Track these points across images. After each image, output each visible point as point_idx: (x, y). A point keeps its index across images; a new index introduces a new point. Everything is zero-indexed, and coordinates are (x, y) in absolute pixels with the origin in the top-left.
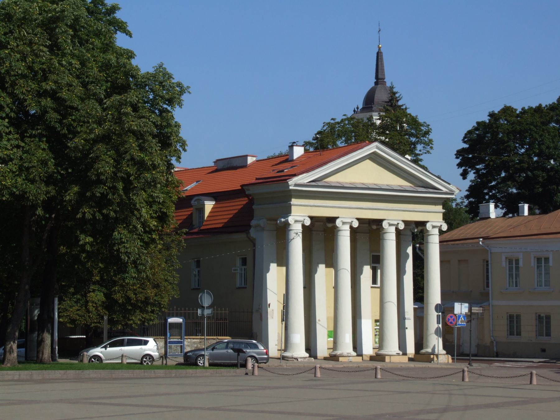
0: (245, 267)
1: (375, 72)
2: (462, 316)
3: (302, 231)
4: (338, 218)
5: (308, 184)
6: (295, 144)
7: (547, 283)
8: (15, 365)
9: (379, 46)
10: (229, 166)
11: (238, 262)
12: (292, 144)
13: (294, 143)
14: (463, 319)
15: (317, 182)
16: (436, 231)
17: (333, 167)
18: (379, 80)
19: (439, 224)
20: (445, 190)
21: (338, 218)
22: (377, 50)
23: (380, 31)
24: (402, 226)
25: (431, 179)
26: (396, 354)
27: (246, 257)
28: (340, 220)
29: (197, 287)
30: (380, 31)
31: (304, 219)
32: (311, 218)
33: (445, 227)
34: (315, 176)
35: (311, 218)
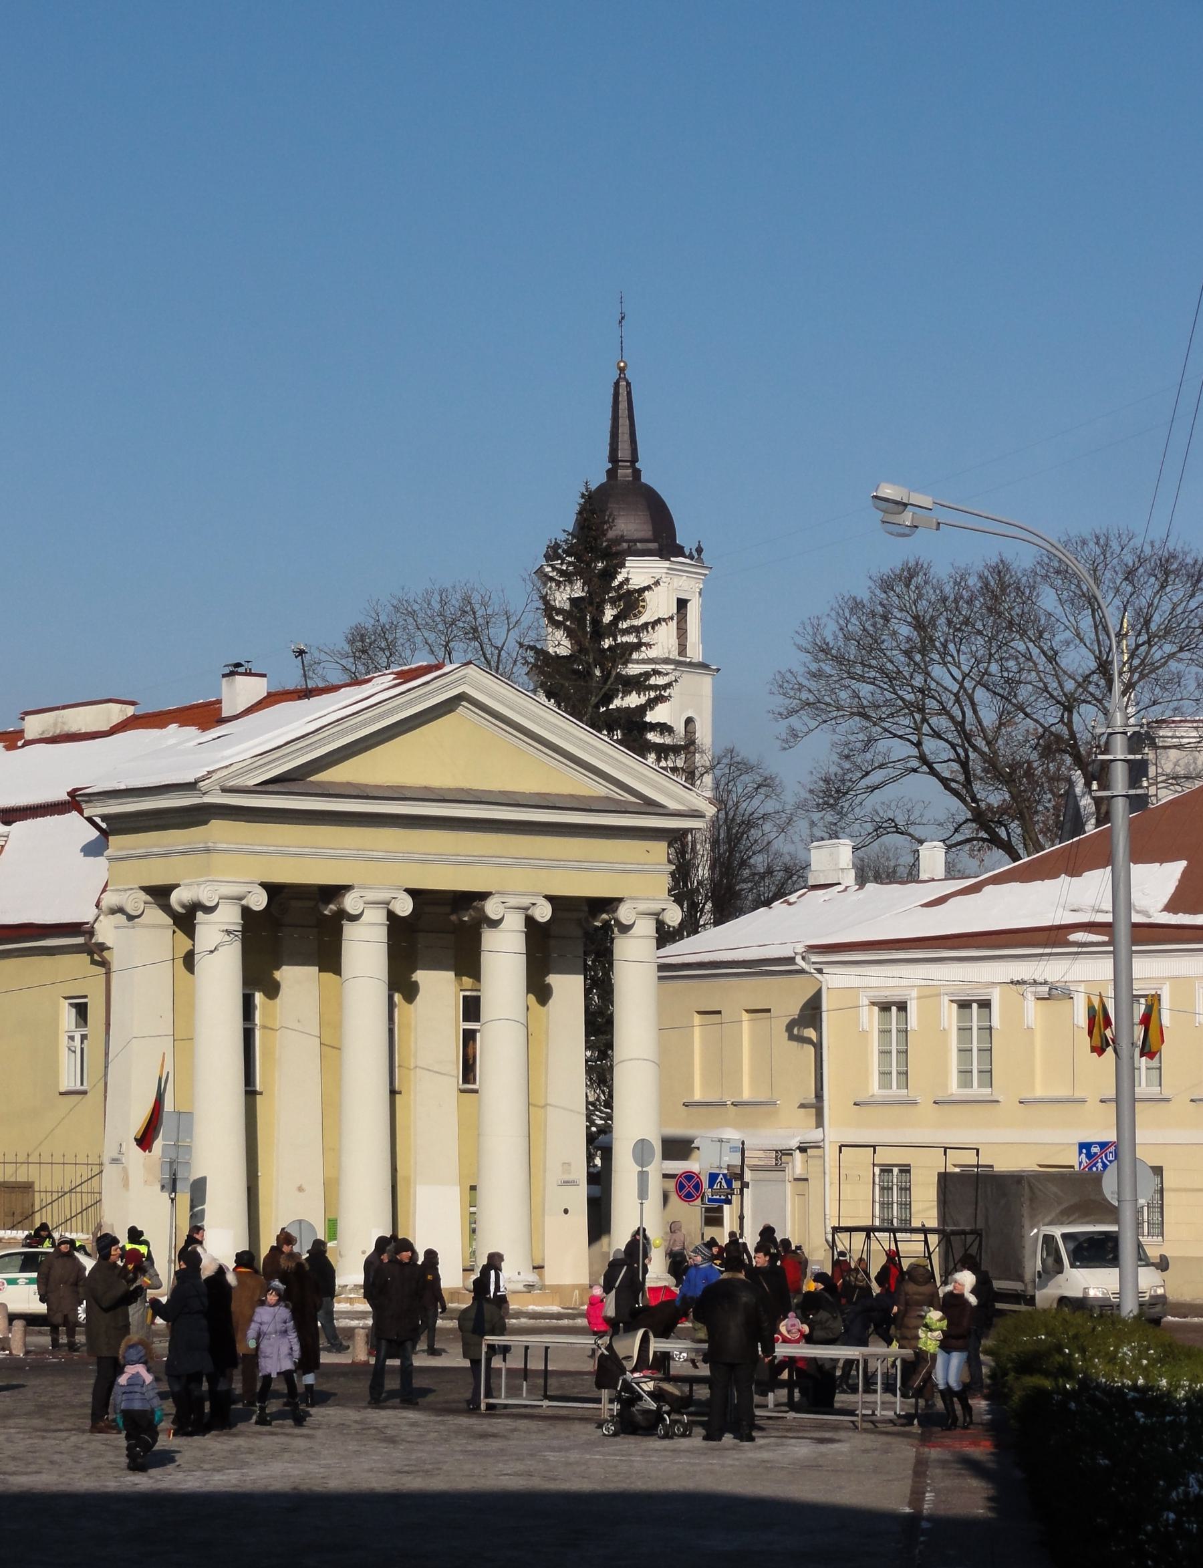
0: (84, 1031)
1: (608, 440)
2: (721, 1176)
3: (243, 926)
4: (348, 888)
5: (259, 788)
6: (241, 670)
7: (987, 1075)
8: (1122, 1373)
9: (618, 364)
10: (58, 732)
11: (68, 1016)
12: (231, 668)
13: (238, 665)
14: (724, 1183)
15: (286, 784)
16: (646, 928)
17: (333, 741)
18: (620, 464)
19: (656, 907)
20: (672, 805)
22: (615, 375)
23: (623, 318)
24: (544, 913)
25: (638, 778)
26: (524, 1289)
27: (479, 994)
28: (358, 895)
29: (78, 1087)
30: (623, 318)
32: (272, 889)
33: (674, 916)
34: (282, 764)
35: (272, 889)
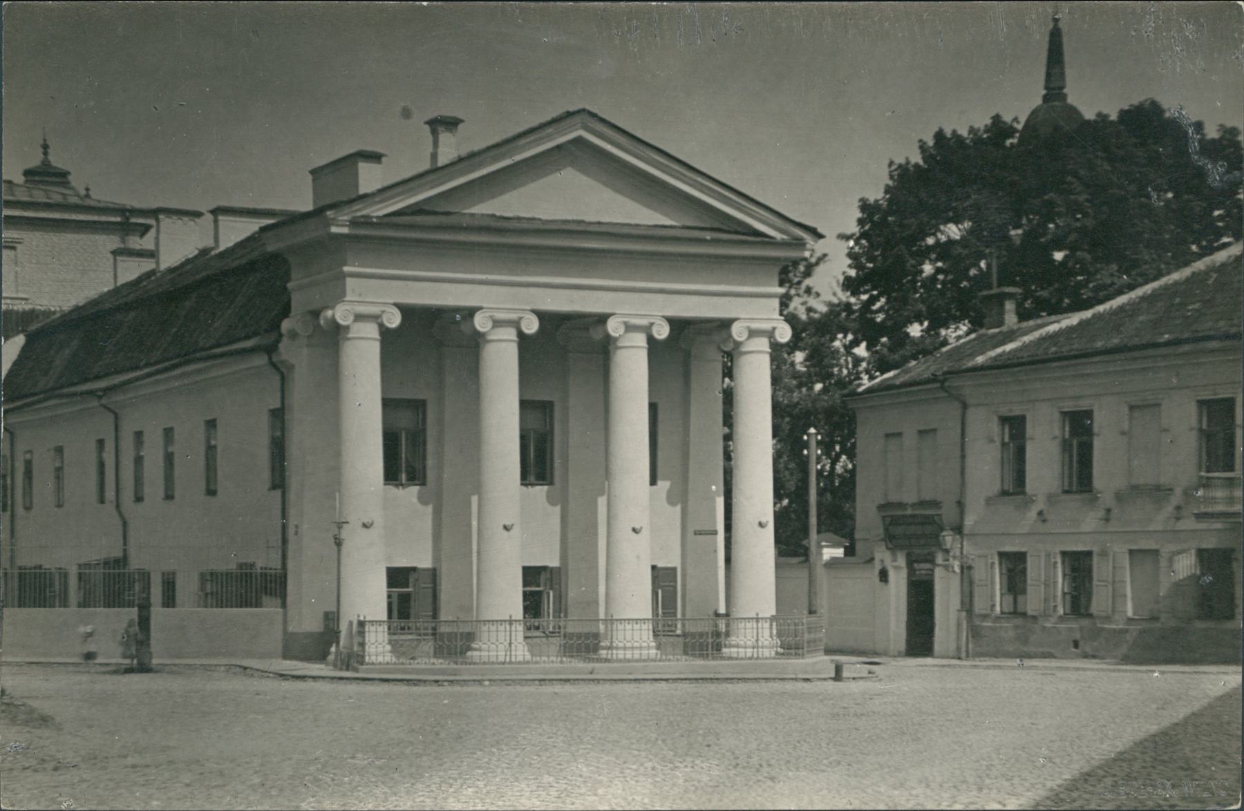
19: (766, 326)
20: (778, 236)
21: (480, 308)
31: (383, 312)
